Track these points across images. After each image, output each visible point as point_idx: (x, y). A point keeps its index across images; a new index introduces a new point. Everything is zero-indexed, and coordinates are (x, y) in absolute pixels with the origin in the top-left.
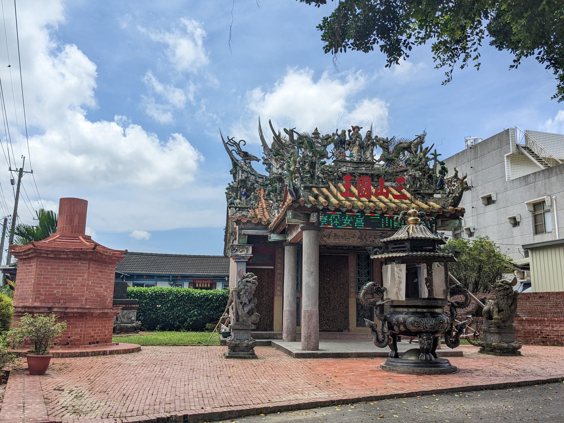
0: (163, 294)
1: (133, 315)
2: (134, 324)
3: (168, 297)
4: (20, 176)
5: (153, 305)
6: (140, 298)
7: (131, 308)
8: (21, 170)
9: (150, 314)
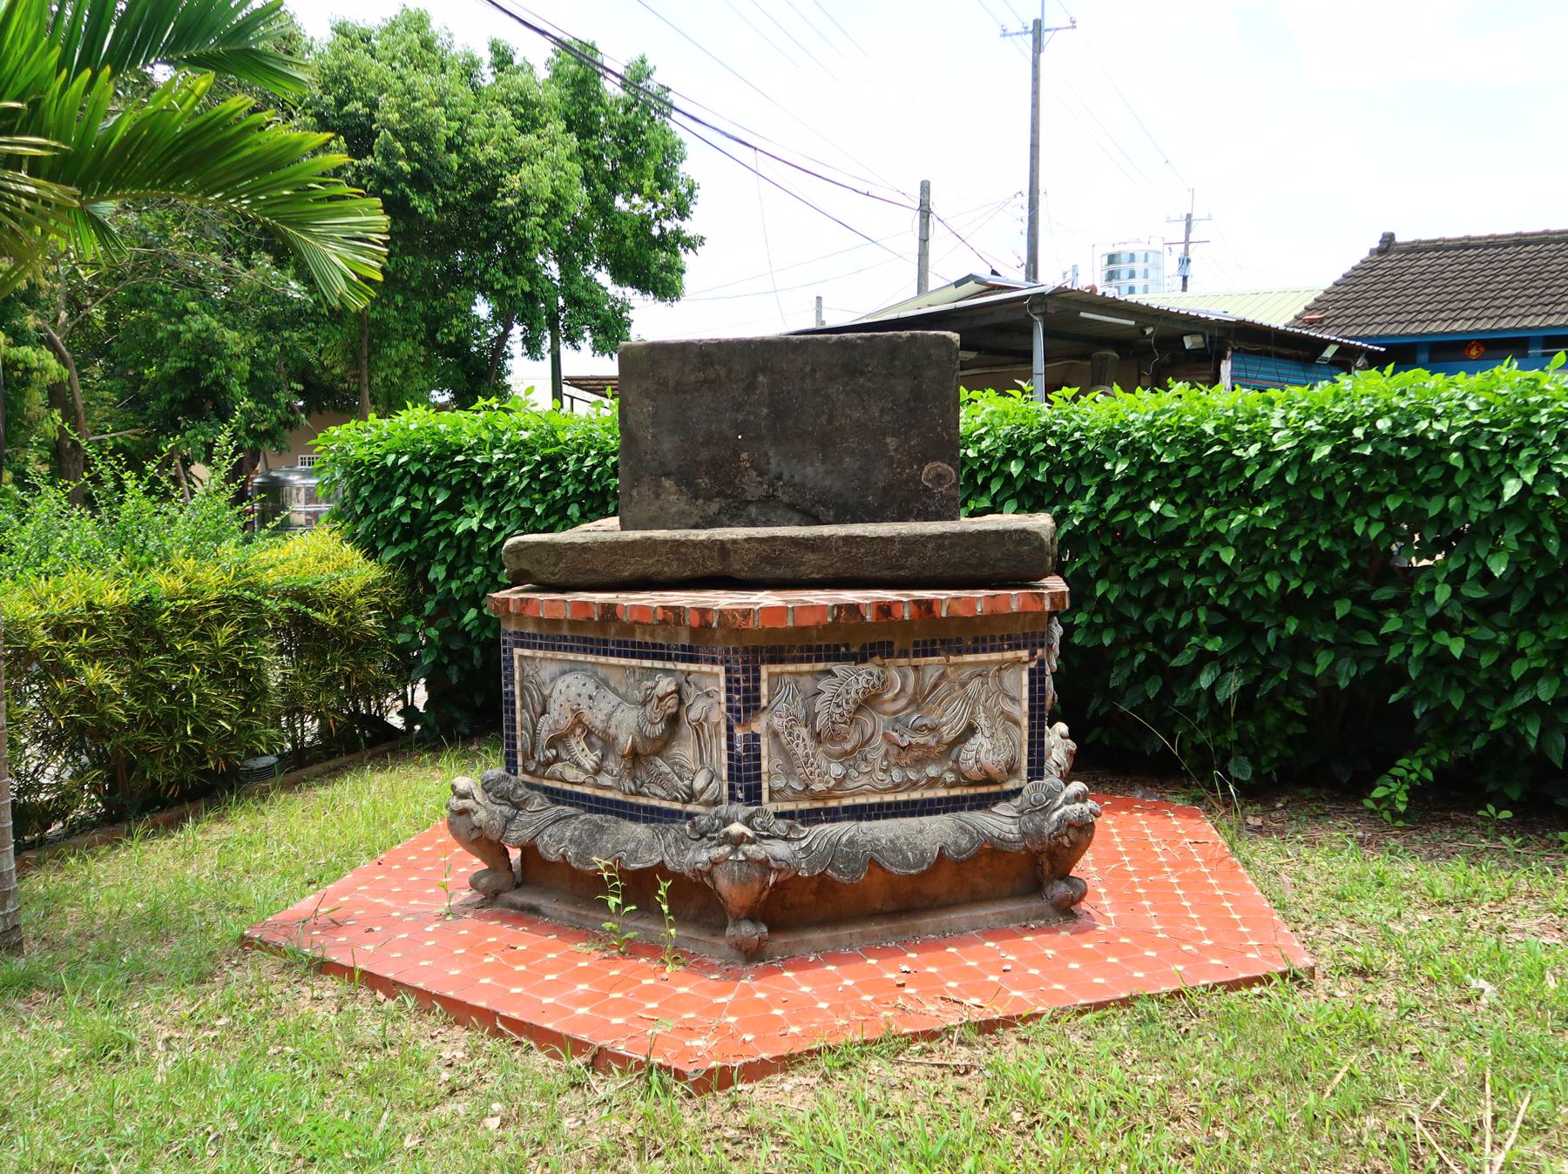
0: (1431, 450)
1: (992, 711)
2: (1001, 822)
3: (1486, 473)
5: (1319, 562)
6: (1194, 494)
7: (937, 637)
8: (1038, 24)
9: (1300, 648)
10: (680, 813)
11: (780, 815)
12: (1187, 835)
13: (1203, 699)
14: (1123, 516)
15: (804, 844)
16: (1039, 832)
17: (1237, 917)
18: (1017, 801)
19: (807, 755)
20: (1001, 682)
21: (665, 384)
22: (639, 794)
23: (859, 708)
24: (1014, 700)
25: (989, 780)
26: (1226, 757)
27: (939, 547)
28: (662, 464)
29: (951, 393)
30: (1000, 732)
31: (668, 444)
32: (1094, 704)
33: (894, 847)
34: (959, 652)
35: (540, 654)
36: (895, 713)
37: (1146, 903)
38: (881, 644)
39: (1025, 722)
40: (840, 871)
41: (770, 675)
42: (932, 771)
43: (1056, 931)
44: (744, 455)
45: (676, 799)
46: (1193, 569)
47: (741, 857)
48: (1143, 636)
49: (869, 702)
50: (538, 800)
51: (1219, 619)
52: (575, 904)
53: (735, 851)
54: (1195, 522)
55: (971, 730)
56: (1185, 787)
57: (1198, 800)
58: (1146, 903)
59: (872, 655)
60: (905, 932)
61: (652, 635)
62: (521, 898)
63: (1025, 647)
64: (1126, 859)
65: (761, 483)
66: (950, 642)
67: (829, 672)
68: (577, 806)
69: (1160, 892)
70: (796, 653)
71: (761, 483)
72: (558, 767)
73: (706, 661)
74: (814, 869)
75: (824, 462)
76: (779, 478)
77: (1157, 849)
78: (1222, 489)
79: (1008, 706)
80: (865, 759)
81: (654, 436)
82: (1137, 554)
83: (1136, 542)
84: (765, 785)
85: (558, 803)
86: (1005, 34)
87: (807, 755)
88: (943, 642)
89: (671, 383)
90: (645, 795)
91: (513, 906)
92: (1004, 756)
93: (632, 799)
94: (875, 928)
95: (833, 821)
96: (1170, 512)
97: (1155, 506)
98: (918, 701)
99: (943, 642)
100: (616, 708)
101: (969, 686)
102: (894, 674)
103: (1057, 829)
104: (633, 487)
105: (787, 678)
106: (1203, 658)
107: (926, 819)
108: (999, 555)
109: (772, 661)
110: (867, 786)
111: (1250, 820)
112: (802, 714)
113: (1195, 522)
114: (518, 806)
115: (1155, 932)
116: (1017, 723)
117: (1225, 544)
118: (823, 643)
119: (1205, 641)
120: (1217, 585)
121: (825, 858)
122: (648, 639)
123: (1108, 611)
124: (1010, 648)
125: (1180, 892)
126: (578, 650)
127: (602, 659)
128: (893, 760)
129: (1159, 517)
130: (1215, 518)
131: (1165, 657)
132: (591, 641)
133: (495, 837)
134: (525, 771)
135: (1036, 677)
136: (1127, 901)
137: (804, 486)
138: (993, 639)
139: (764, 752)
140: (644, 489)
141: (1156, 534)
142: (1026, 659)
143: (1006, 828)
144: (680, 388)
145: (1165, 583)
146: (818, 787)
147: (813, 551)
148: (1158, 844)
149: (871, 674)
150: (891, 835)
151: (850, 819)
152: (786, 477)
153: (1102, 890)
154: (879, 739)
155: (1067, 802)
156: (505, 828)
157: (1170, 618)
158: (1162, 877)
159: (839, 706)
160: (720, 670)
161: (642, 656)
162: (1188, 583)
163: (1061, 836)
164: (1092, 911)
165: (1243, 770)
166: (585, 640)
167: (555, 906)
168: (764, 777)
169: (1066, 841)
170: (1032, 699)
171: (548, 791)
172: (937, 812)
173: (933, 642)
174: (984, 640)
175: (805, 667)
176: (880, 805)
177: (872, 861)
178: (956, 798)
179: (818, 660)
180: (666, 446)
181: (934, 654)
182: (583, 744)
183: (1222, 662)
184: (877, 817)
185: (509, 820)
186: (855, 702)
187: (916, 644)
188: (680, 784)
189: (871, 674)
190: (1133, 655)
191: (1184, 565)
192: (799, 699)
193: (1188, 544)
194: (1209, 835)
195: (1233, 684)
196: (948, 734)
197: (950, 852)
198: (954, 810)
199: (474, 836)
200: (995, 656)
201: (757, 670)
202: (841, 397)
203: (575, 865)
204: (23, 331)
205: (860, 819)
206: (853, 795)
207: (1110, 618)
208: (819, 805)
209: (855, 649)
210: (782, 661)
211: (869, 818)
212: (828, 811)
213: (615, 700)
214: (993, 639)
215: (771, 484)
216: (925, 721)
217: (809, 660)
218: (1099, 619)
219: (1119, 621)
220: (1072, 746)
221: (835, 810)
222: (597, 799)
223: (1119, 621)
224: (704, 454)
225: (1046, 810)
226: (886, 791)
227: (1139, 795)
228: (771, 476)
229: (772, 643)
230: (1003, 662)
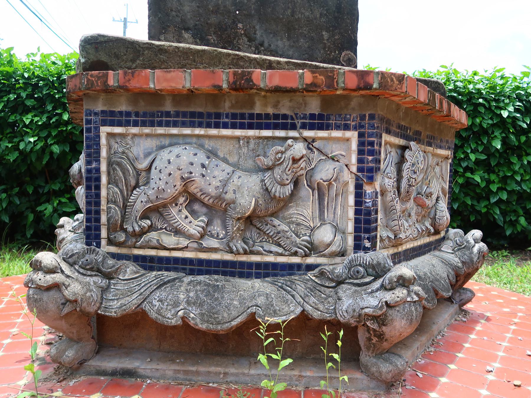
8: (125, 19)
10: (299, 266)
22: (252, 253)
35: (134, 130)
45: (295, 254)
50: (130, 270)
52: (173, 361)
61: (276, 105)
62: (112, 364)
68: (176, 270)
72: (153, 235)
73: (338, 128)
75: (289, 39)
76: (262, 44)
85: (152, 269)
86: (114, 20)
90: (258, 253)
91: (104, 373)
93: (244, 258)
100: (230, 175)
114: (108, 276)
122: (270, 111)
126: (184, 125)
127: (213, 132)
132: (201, 115)
133: (92, 309)
134: (110, 242)
152: (266, 44)
156: (102, 298)
161: (260, 127)
166: (193, 115)
167: (154, 366)
171: (137, 259)
182: (185, 212)
185: (104, 290)
188: (298, 240)
199: (67, 310)
203: (203, 326)
213: (229, 169)
222: (201, 262)
224: (213, 19)
228: (257, 42)
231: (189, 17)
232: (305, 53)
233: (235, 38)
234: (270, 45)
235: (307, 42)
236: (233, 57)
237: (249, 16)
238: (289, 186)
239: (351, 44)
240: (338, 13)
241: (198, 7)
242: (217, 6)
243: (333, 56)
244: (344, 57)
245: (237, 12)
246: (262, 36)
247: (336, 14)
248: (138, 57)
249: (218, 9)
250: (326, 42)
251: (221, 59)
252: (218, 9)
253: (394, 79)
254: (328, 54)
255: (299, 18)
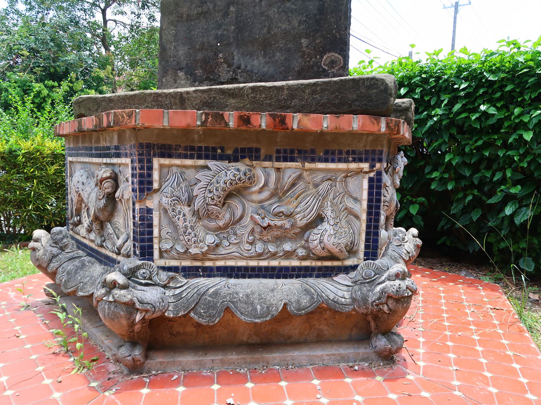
2: (337, 290)
4: (456, 12)
6: (508, 101)
8: (457, 3)
11: (164, 268)
12: (490, 303)
13: (506, 223)
14: (463, 115)
15: (178, 291)
16: (365, 299)
17: (525, 381)
18: (353, 274)
19: (186, 227)
20: (346, 186)
21: (182, 17)
22: (102, 246)
23: (229, 195)
24: (356, 200)
25: (332, 257)
26: (518, 257)
27: (314, 92)
28: (178, 63)
29: (343, 7)
30: (343, 222)
31: (182, 51)
32: (442, 224)
33: (248, 300)
34: (313, 160)
36: (261, 202)
37: (452, 356)
38: (250, 150)
39: (364, 217)
40: (200, 315)
41: (161, 166)
42: (287, 247)
43: (372, 375)
44: (221, 55)
46: (506, 146)
47: (111, 299)
48: (472, 186)
49: (235, 192)
51: (520, 176)
53: (108, 293)
54: (508, 118)
55: (320, 219)
56: (491, 272)
57: (498, 280)
58: (452, 356)
59: (243, 157)
60: (257, 362)
63: (366, 161)
64: (445, 315)
65: (229, 71)
66: (306, 152)
67: (207, 167)
69: (465, 346)
70: (181, 151)
71: (229, 71)
74: (178, 312)
75: (264, 57)
76: (239, 68)
77: (468, 311)
78: (527, 97)
79: (350, 204)
80: (235, 234)
81: (175, 47)
82: (471, 139)
83: (472, 131)
84: (156, 246)
85: (79, 248)
86: (445, 7)
87: (186, 227)
88: (300, 152)
89: (185, 16)
92: (344, 241)
94: (233, 357)
95: (209, 276)
96: (492, 111)
97: (483, 108)
98: (278, 194)
99: (300, 152)
101: (321, 187)
102: (259, 172)
103: (379, 299)
104: (163, 77)
105: (175, 169)
106: (508, 198)
107: (281, 281)
108: (355, 97)
109: (162, 156)
110: (233, 255)
111: (531, 295)
112: (184, 197)
113: (508, 118)
115: (453, 388)
116: (357, 217)
117: (527, 129)
118: (203, 145)
119: (509, 188)
120: (520, 155)
121: (190, 304)
123: (452, 172)
124: (354, 161)
125: (479, 348)
128: (257, 236)
129: (485, 113)
130: (521, 114)
131: (484, 198)
135: (376, 186)
136: (437, 352)
137: (252, 72)
138: (340, 152)
139: (156, 222)
140: (169, 78)
141: (483, 126)
142: (366, 169)
143: (340, 293)
144: (189, 18)
145: (487, 154)
146: (194, 251)
147: (233, 98)
148: (469, 306)
149: (238, 170)
150: (249, 291)
151: (222, 276)
152: (243, 67)
153: (421, 340)
154: (247, 220)
155: (389, 279)
157: (488, 175)
158: (468, 333)
159: (210, 192)
160: (128, 161)
162: (501, 153)
163: (382, 304)
164: (409, 360)
165: (528, 265)
168: (156, 241)
169: (385, 308)
170: (370, 200)
172: (291, 277)
173: (292, 151)
174: (333, 153)
175: (189, 162)
176: (246, 268)
177: (228, 309)
178: (306, 268)
179: (199, 157)
180: (181, 53)
181: (293, 160)
183: (521, 202)
184: (244, 277)
185: (54, 256)
186: (224, 190)
187: (278, 151)
189: (238, 170)
190: (465, 196)
191: (499, 143)
192: (183, 185)
193: (503, 131)
194: (504, 304)
195: (527, 215)
196: (301, 221)
197: (292, 308)
198: (305, 276)
200: (342, 166)
201: (150, 161)
202: (276, 16)
204: (103, 91)
205: (230, 276)
206: (224, 259)
207: (453, 176)
208: (198, 264)
209: (229, 152)
210: (170, 156)
211: (237, 277)
212: (205, 269)
214: (340, 152)
215: (234, 72)
216: (282, 209)
217: (192, 157)
218: (446, 176)
219: (459, 178)
220: (419, 242)
221: (211, 269)
223: (459, 178)
224: (200, 56)
225: (372, 282)
226: (251, 258)
227: (463, 274)
229: (161, 142)
230: (348, 171)
231: (182, 59)
232: (281, 66)
233: (216, 68)
234: (246, 66)
235: (284, 54)
236: (153, 95)
237: (229, 44)
238: (103, 200)
239: (341, 45)
240: (320, 14)
241: (189, 49)
242: (203, 44)
243: (314, 62)
244: (325, 61)
245: (219, 44)
246: (239, 60)
247: (318, 17)
248: (99, 107)
249: (203, 46)
250: (305, 49)
251: (146, 98)
252: (203, 46)
253: (125, 116)
254: (308, 61)
255: (275, 33)
